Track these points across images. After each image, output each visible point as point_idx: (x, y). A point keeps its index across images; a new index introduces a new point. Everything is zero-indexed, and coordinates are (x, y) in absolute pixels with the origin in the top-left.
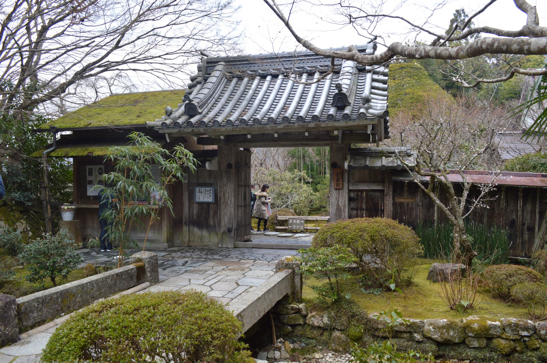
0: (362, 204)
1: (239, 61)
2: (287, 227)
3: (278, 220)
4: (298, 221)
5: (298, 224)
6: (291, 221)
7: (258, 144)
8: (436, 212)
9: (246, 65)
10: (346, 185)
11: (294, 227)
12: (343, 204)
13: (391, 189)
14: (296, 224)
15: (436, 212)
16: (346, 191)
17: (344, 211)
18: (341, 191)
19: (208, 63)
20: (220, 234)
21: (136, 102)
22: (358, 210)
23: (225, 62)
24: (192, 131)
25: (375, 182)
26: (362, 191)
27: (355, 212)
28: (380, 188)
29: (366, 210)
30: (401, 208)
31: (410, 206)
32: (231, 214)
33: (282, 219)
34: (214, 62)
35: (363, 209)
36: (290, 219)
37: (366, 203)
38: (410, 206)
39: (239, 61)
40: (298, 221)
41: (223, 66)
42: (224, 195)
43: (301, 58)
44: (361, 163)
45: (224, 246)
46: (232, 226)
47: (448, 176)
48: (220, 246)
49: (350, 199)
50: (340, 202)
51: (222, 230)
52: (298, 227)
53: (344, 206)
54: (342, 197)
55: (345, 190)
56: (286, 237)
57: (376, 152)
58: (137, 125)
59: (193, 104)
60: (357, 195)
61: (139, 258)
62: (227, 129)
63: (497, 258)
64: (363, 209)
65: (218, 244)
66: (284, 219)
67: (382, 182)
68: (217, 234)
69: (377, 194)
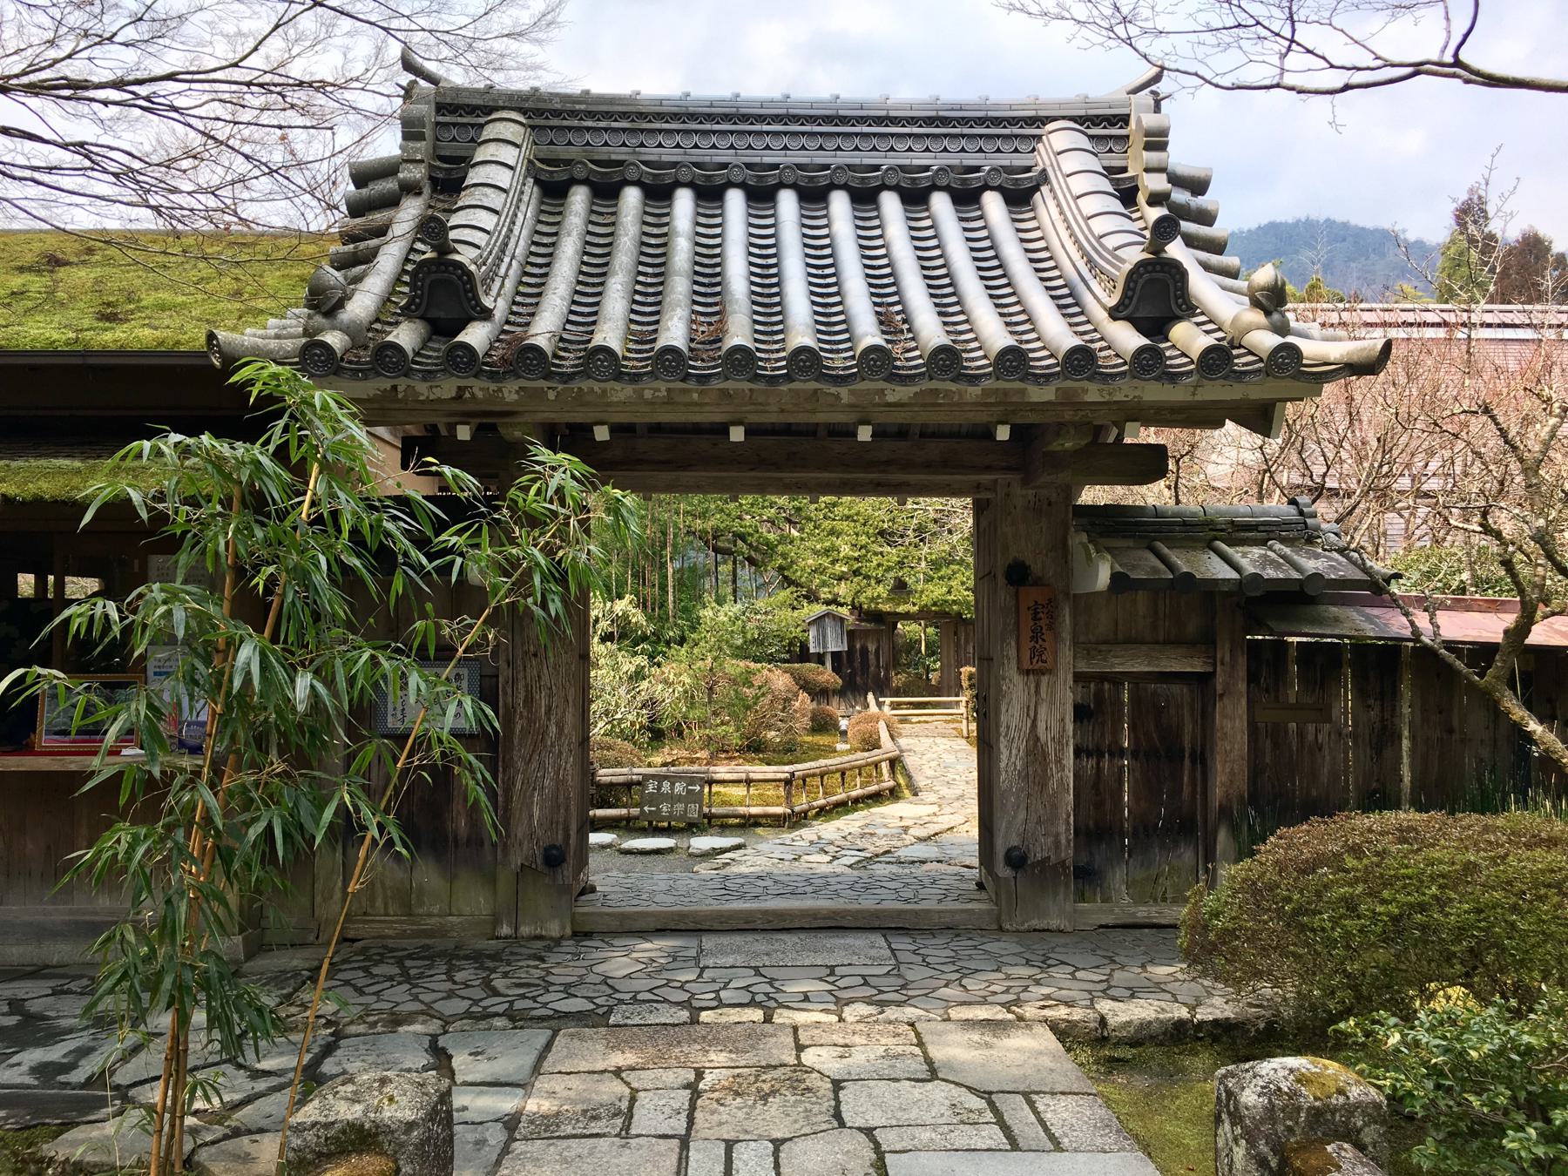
0: (1117, 732)
1: (591, 115)
2: (635, 811)
3: (599, 786)
4: (679, 788)
5: (679, 798)
6: (651, 787)
7: (687, 476)
8: (1406, 760)
9: (624, 137)
10: (1066, 654)
11: (665, 808)
12: (1055, 732)
13: (1242, 671)
14: (672, 798)
15: (1406, 760)
16: (1065, 678)
17: (1059, 761)
18: (1045, 679)
19: (441, 108)
20: (505, 878)
21: (55, 262)
22: (1100, 756)
23: (523, 111)
24: (459, 397)
25: (1175, 642)
26: (1116, 679)
27: (1092, 762)
28: (1197, 666)
29: (1135, 754)
30: (1276, 745)
31: (1311, 737)
32: (559, 783)
33: (615, 779)
34: (472, 110)
35: (1122, 753)
36: (647, 777)
37: (1132, 728)
38: (1311, 737)
39: (591, 115)
40: (679, 788)
41: (522, 130)
42: (529, 700)
43: (866, 129)
44: (1146, 566)
45: (525, 930)
46: (567, 837)
47: (1442, 617)
48: (505, 930)
49: (1081, 713)
50: (1041, 726)
51: (517, 860)
52: (680, 807)
53: (1060, 742)
54: (1052, 703)
55: (1061, 674)
56: (658, 852)
57: (1184, 524)
58: (121, 353)
59: (460, 265)
60: (1099, 696)
61: (354, 1128)
62: (640, 393)
63: (130, 732)
64: (1122, 753)
65: (496, 921)
66: (621, 779)
67: (1206, 642)
68: (492, 880)
69: (1176, 689)
